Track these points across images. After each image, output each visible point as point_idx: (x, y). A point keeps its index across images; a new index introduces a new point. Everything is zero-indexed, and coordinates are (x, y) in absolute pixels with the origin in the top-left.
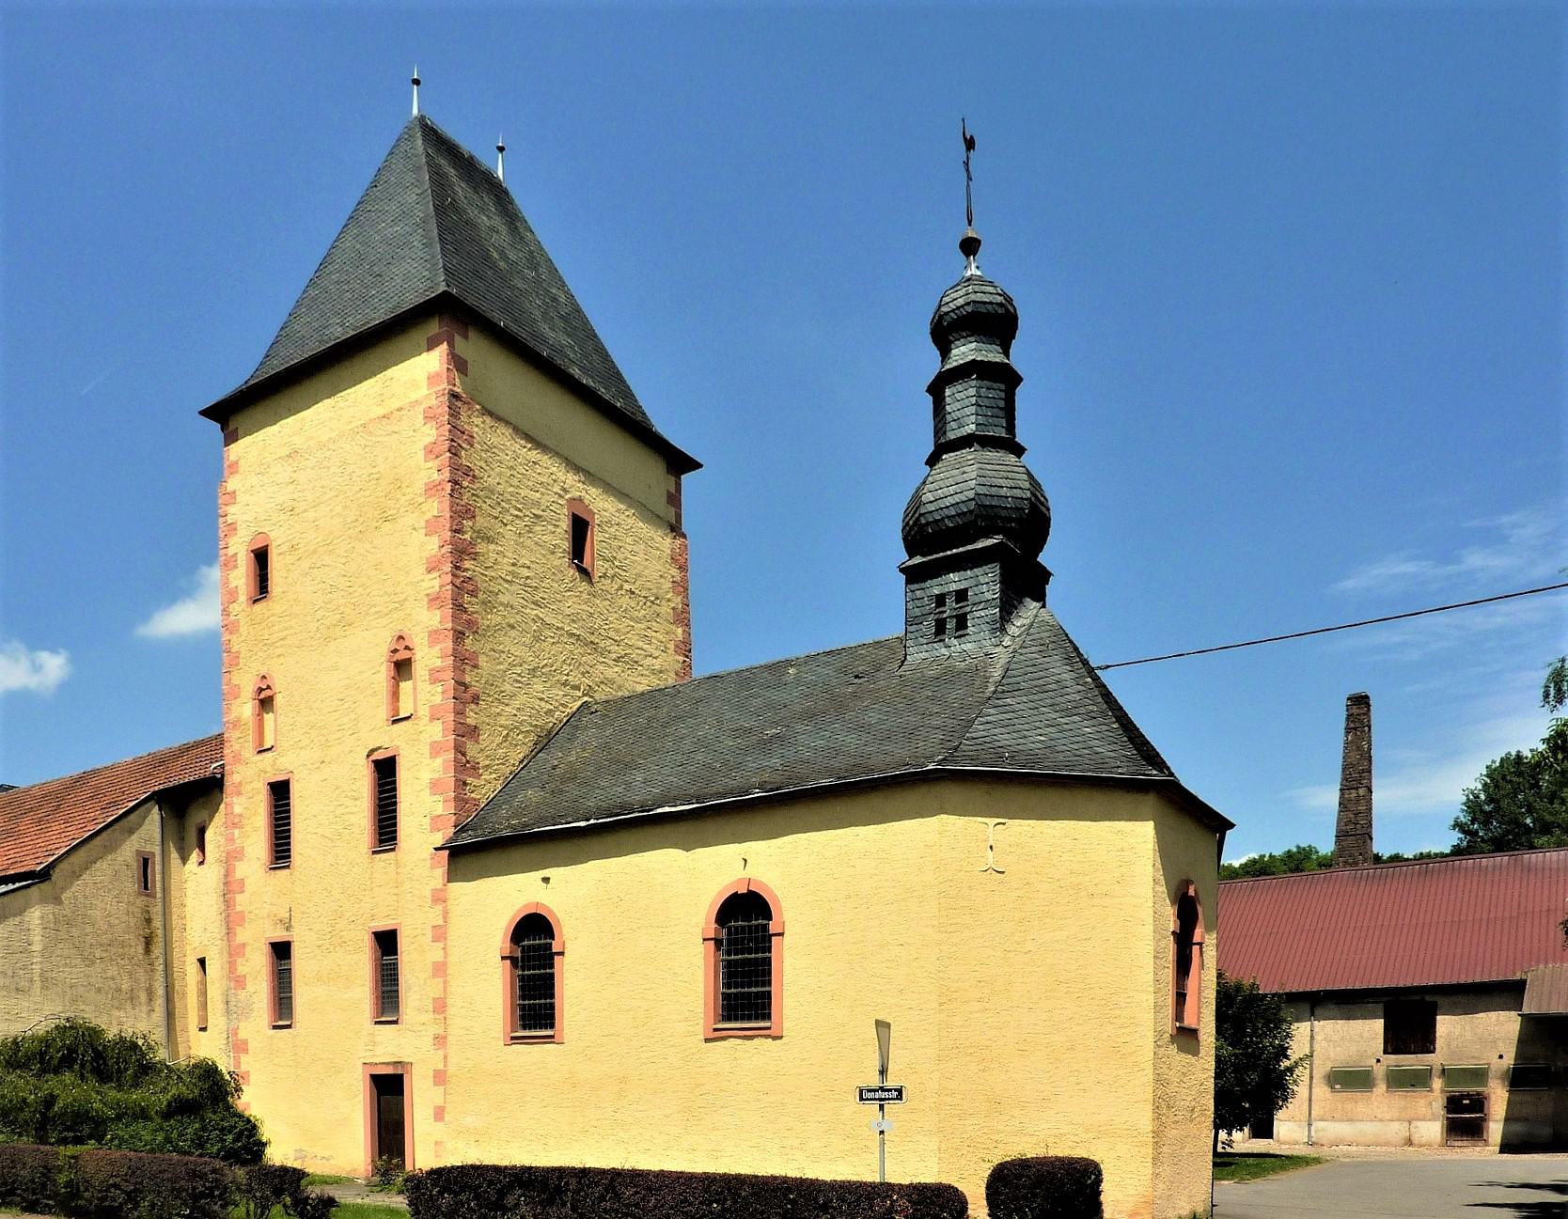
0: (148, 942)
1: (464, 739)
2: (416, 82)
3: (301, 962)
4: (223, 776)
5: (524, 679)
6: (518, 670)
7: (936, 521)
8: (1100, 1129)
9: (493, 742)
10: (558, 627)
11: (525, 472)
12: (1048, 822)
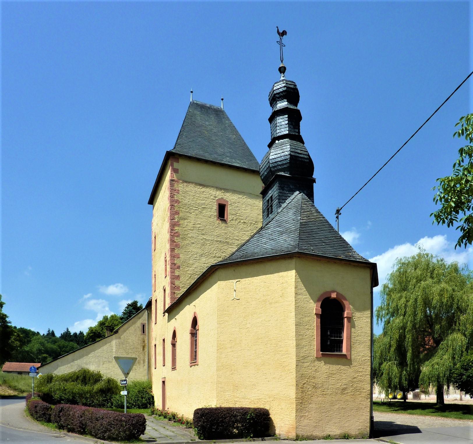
0: (144, 347)
1: (174, 280)
2: (192, 92)
5: (198, 258)
6: (195, 256)
8: (275, 397)
9: (185, 279)
10: (212, 240)
11: (199, 196)
12: (255, 278)
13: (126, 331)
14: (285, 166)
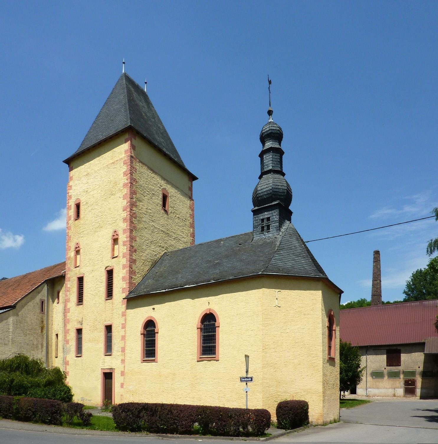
1: (132, 264)
2: (124, 63)
3: (85, 335)
4: (65, 275)
7: (261, 196)
8: (308, 391)
11: (150, 180)
13: (24, 307)
14: (282, 197)
